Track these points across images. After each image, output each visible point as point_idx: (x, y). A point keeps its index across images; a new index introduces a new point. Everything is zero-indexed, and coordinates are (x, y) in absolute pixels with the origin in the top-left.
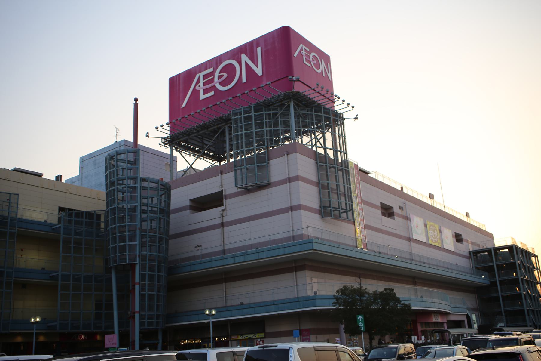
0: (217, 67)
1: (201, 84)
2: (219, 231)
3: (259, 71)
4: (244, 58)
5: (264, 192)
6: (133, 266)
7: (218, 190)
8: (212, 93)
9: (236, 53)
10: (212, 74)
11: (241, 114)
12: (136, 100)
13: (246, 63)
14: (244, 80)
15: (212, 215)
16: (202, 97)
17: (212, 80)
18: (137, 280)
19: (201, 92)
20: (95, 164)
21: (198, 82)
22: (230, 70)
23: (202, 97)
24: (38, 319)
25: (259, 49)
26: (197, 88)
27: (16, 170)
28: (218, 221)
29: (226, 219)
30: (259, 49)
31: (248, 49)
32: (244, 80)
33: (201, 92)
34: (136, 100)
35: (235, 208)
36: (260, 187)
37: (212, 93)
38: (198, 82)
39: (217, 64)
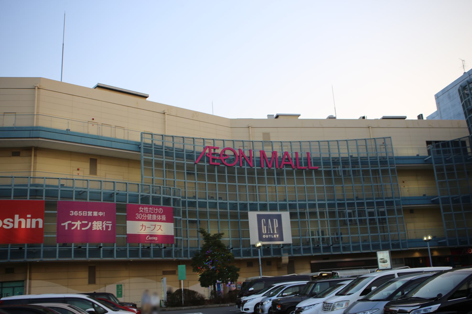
20: (449, 97)
24: (430, 238)
27: (384, 118)
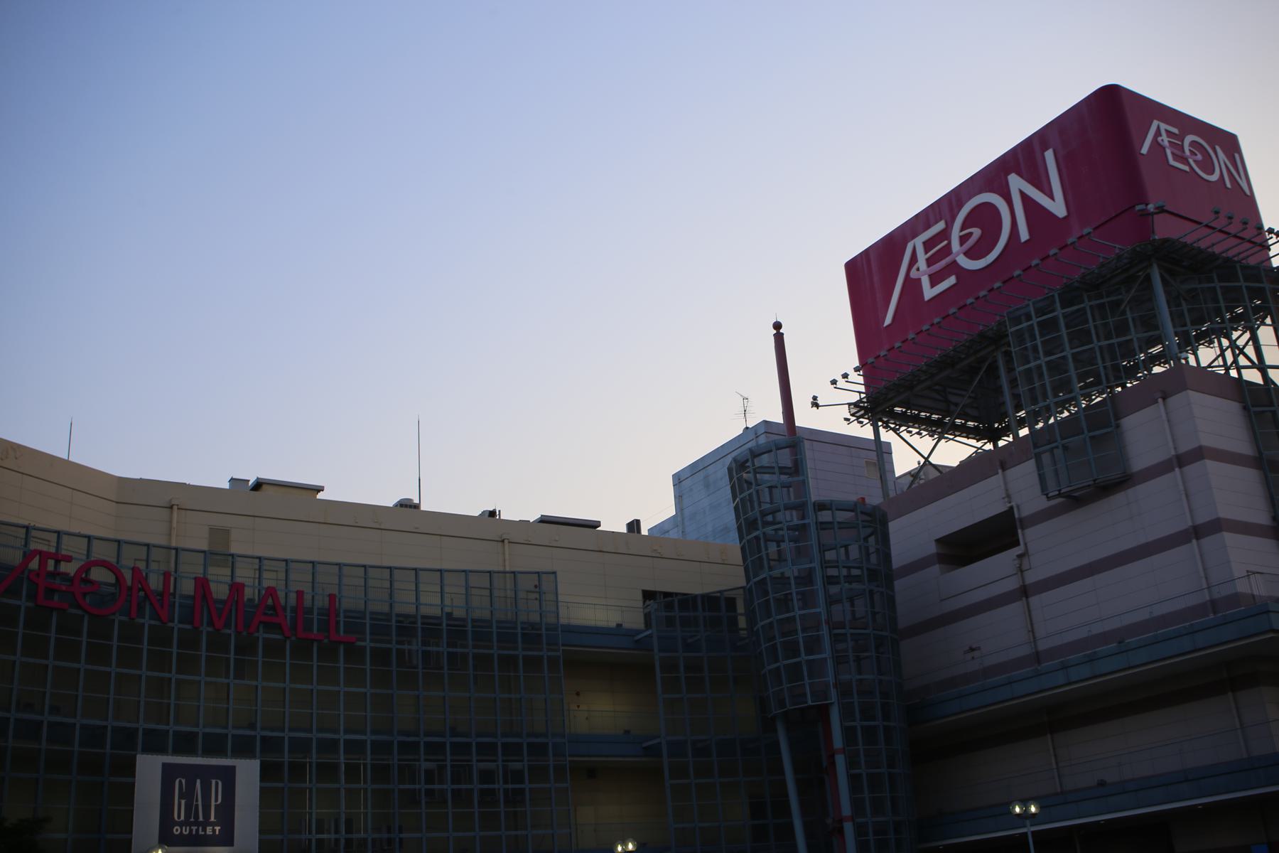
0: (953, 218)
1: (922, 263)
2: (1016, 608)
3: (1057, 207)
4: (1016, 183)
5: (1119, 498)
6: (824, 711)
7: (999, 508)
8: (952, 280)
9: (993, 177)
10: (945, 235)
11: (1029, 318)
12: (777, 326)
13: (1023, 194)
14: (1024, 235)
15: (995, 571)
16: (929, 293)
17: (947, 250)
18: (838, 742)
19: (925, 281)
20: (707, 486)
21: (914, 259)
22: (986, 218)
23: (929, 293)
24: (630, 847)
25: (1049, 155)
26: (914, 274)
27: (545, 520)
28: (1012, 584)
29: (1031, 578)
30: (1049, 155)
31: (1023, 159)
32: (1024, 235)
33: (925, 281)
34: (777, 326)
35: (1053, 545)
36: (1106, 489)
37: (952, 280)
38: (914, 259)
39: (951, 209)
